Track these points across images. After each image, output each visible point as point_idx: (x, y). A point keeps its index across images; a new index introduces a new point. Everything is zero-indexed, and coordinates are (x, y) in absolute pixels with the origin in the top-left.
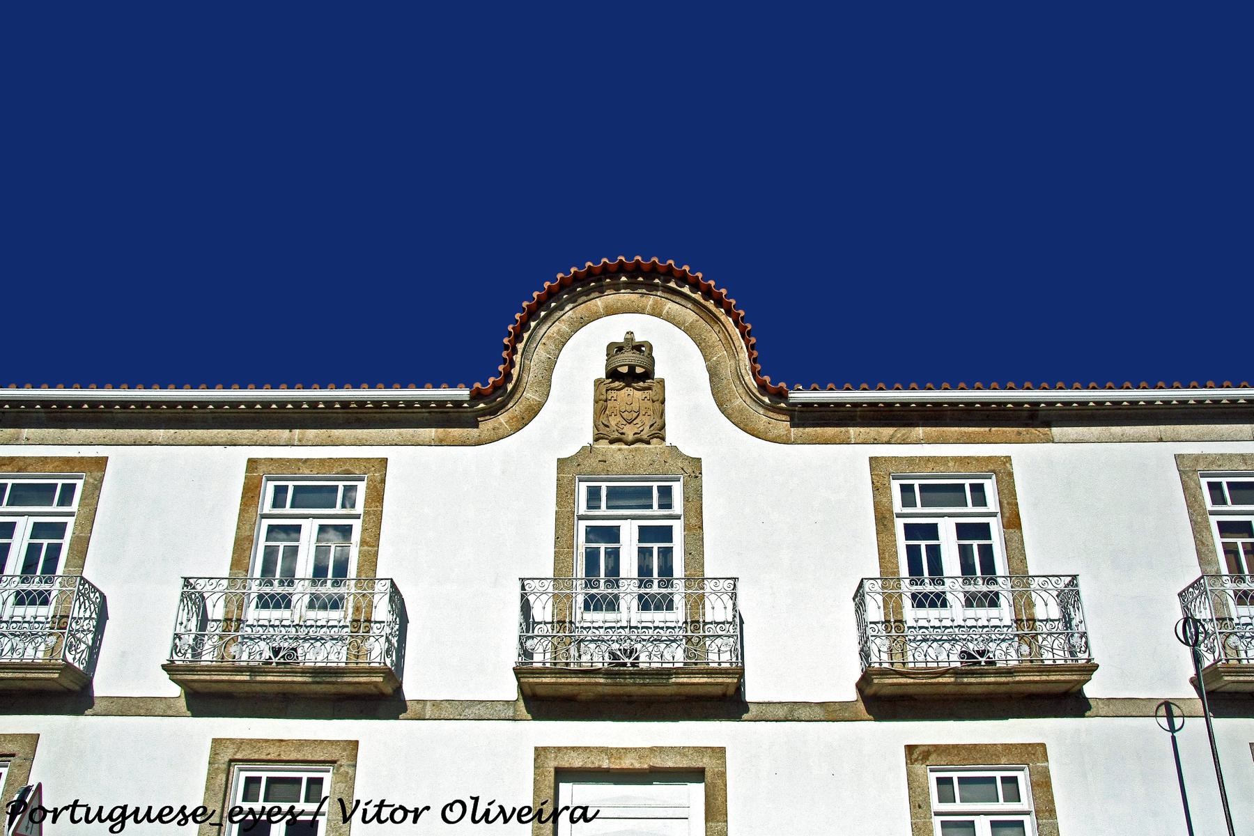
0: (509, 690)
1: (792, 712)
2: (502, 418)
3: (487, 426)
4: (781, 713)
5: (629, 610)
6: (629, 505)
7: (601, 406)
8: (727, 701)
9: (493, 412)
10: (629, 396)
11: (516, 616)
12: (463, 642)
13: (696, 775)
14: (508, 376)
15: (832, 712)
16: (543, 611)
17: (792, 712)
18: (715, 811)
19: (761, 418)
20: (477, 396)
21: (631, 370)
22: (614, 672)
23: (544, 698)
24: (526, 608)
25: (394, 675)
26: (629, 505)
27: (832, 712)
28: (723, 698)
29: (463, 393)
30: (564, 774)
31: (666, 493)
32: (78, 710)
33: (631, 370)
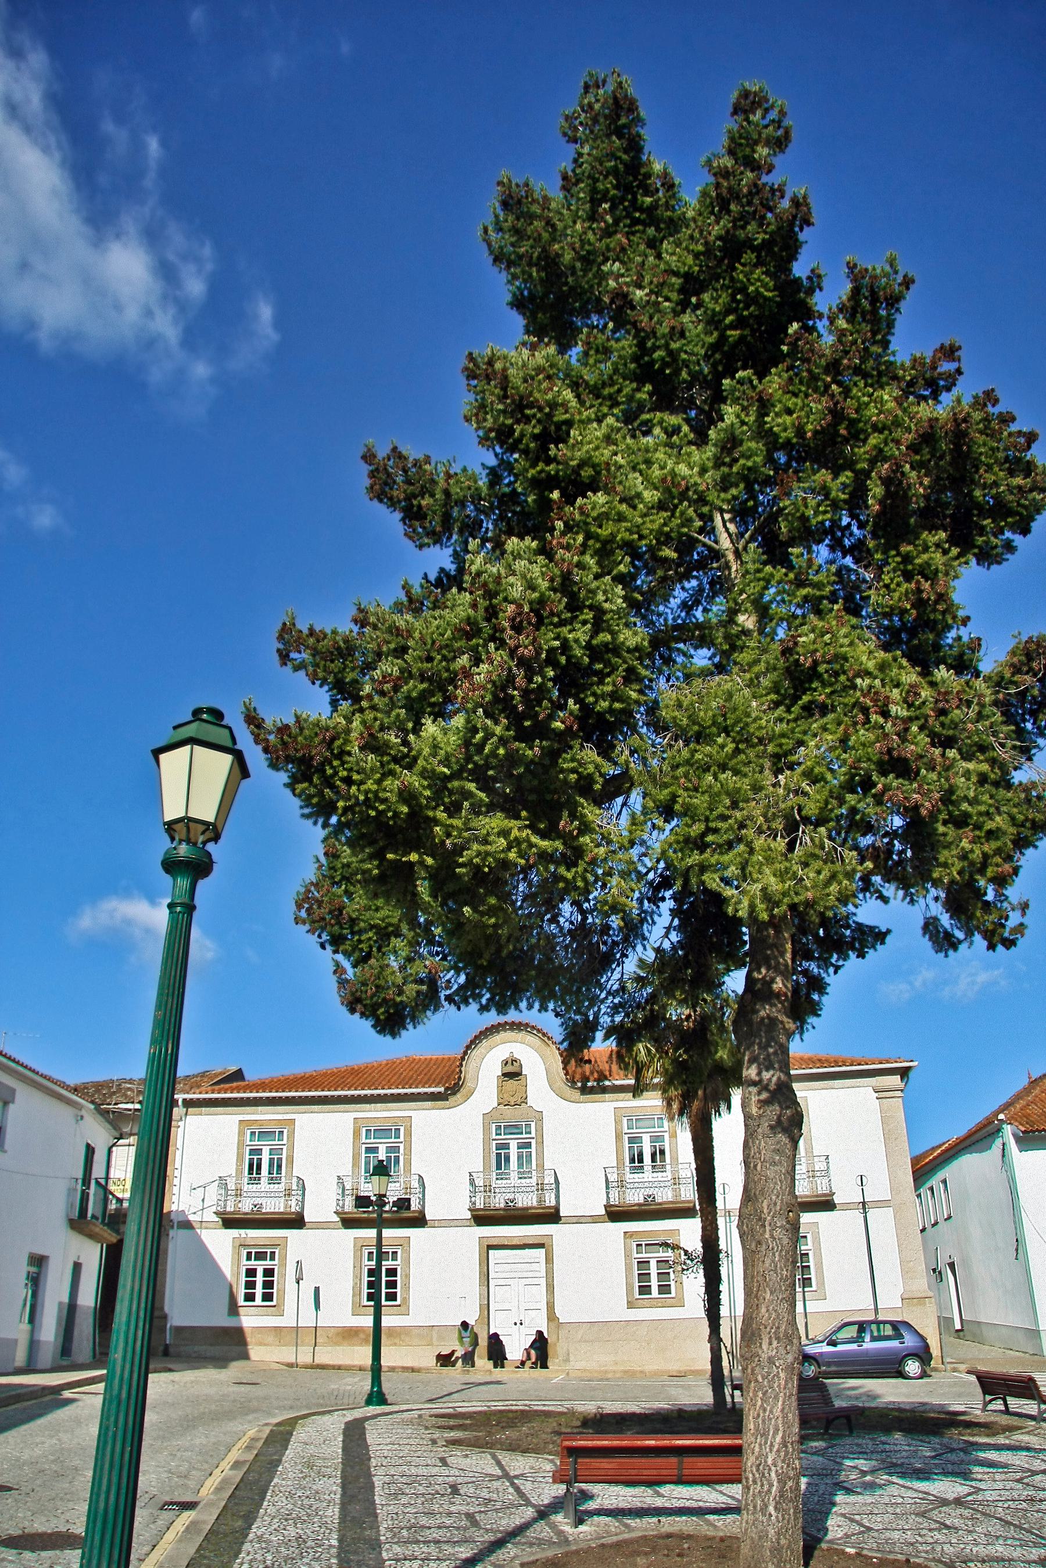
0: (468, 1215)
1: (579, 1220)
2: (458, 1095)
3: (452, 1099)
4: (575, 1220)
5: (514, 1179)
6: (512, 1135)
7: (500, 1088)
8: (553, 1216)
9: (454, 1094)
10: (511, 1084)
11: (468, 1186)
12: (447, 1197)
13: (541, 1246)
14: (460, 1078)
15: (595, 1219)
16: (479, 1182)
17: (579, 1220)
18: (549, 1260)
19: (568, 1091)
20: (447, 1089)
21: (512, 1073)
22: (507, 1208)
23: (482, 1218)
24: (472, 1182)
25: (557, 1209)
26: (512, 1135)
27: (595, 1219)
28: (551, 1214)
29: (442, 1089)
30: (490, 1247)
31: (528, 1126)
32: (301, 1228)
33: (512, 1073)
